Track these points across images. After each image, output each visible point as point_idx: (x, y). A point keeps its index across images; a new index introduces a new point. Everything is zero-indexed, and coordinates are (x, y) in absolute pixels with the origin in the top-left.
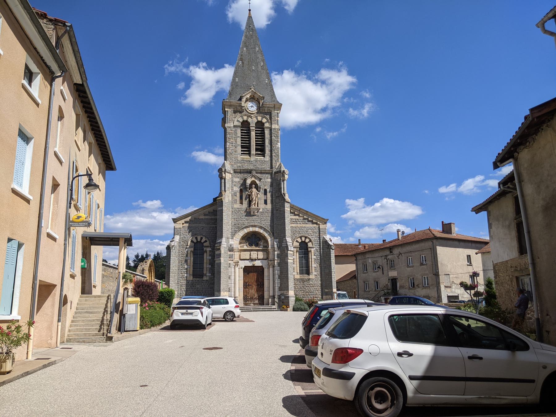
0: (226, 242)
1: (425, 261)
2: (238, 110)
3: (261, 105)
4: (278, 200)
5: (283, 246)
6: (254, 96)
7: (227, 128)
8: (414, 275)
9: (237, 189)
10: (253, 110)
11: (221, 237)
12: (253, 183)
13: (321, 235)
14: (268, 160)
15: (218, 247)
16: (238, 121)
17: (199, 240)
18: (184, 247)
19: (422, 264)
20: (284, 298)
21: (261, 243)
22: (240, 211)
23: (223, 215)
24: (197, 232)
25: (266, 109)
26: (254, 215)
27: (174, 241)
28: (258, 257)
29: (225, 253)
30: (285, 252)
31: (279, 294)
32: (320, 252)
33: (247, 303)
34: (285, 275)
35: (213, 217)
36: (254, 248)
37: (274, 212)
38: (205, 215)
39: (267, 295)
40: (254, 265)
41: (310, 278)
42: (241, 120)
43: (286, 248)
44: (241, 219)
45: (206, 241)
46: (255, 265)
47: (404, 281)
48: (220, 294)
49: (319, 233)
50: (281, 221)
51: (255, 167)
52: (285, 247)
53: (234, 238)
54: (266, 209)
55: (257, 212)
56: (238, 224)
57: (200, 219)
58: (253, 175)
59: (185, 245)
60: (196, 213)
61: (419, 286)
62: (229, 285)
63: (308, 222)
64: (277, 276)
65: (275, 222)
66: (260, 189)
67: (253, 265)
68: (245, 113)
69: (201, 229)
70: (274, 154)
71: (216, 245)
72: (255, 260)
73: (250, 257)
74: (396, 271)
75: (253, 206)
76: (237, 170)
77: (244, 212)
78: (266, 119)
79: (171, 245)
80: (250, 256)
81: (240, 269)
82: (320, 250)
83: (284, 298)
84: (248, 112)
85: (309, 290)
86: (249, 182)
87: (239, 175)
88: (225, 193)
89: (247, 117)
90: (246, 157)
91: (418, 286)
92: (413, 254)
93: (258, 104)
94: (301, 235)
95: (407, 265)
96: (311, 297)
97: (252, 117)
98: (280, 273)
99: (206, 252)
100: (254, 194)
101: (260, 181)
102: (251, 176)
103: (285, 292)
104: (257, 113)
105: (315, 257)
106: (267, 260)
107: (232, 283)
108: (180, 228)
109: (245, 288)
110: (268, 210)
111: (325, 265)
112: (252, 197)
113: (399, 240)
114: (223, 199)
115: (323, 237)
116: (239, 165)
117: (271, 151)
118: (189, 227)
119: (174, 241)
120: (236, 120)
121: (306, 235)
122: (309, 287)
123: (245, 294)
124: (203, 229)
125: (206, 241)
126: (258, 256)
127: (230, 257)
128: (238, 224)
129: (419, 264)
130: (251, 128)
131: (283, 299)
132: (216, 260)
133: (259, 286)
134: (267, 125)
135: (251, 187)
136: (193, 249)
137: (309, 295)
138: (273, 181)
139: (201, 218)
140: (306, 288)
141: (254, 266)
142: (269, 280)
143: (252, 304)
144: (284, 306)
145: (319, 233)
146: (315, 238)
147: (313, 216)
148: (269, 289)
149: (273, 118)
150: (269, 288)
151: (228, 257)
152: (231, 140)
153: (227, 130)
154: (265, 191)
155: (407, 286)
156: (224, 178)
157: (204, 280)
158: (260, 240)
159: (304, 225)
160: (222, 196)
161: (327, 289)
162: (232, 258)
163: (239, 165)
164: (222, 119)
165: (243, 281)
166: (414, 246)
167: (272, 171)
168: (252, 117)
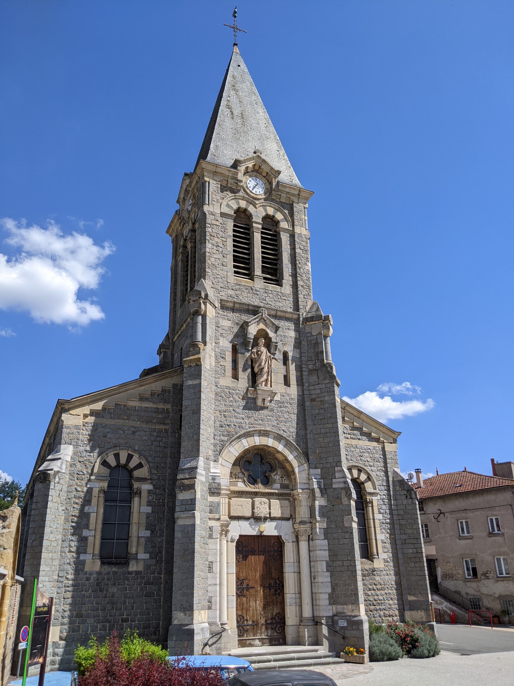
1: (498, 526)
2: (229, 185)
3: (274, 186)
4: (316, 377)
5: (334, 486)
6: (260, 167)
7: (207, 213)
8: (476, 554)
9: (226, 345)
10: (258, 193)
11: (195, 453)
12: (262, 334)
13: (388, 465)
14: (288, 292)
15: (186, 482)
16: (228, 206)
17: (123, 460)
18: (83, 476)
19: (491, 534)
20: (345, 625)
21: (276, 476)
22: (233, 393)
23: (200, 398)
24: (120, 441)
25: (282, 195)
26: (263, 408)
27: (60, 459)
28: (270, 513)
30: (341, 503)
31: (331, 614)
32: (390, 505)
34: (346, 563)
35: (159, 407)
36: (260, 488)
37: (308, 404)
38: (142, 399)
39: (294, 614)
40: (262, 532)
41: (375, 567)
42: (235, 207)
43: (343, 492)
44: (236, 414)
45: (140, 466)
46: (265, 533)
47: (451, 564)
48: (192, 619)
49: (385, 463)
50: (326, 426)
51: (264, 302)
52: (341, 488)
53: (220, 460)
54: (288, 395)
55: (271, 401)
56: (228, 425)
57: (128, 409)
58: (264, 316)
59: (87, 472)
60: (120, 393)
61: (488, 575)
62: (210, 588)
63: (361, 435)
64: (322, 566)
65: (309, 428)
66: (276, 351)
67: (259, 534)
68: (241, 193)
69: (130, 432)
70: (300, 283)
71: (180, 476)
72: (265, 519)
73: (253, 513)
74: (433, 545)
75: (262, 387)
76: (227, 301)
77: (241, 397)
78: (283, 215)
79: (52, 470)
80: (253, 508)
81: (229, 543)
82: (390, 500)
83: (345, 625)
84: (247, 194)
85: (376, 597)
86: (253, 330)
87: (230, 315)
88: (206, 347)
89: (245, 202)
90: (245, 281)
91: (485, 574)
92: (470, 514)
93: (268, 184)
94: (351, 464)
95: (458, 535)
96: (380, 616)
97: (256, 204)
98: (329, 556)
99: (139, 493)
100: (264, 358)
101: (276, 332)
102: (257, 320)
103: (348, 610)
104: (265, 199)
105: (380, 516)
106: (290, 522)
108: (77, 427)
110: (292, 399)
111: (404, 537)
112: (260, 365)
113: (420, 487)
114: (201, 361)
115: (394, 470)
116: (230, 292)
117: (294, 276)
118: (95, 427)
119: (60, 459)
120: (224, 203)
121: (360, 465)
122: (374, 590)
123: (240, 613)
124: (134, 433)
125: (140, 466)
126: (270, 509)
127: (211, 510)
128: (228, 425)
129: (485, 534)
130: (254, 225)
131: (342, 628)
132: (178, 518)
134: (284, 225)
135: (256, 343)
136: (105, 485)
137: (376, 610)
138: (300, 337)
139: (132, 406)
141: (260, 537)
143: (257, 642)
144: (352, 649)
145: (385, 463)
146: (378, 473)
147: (372, 423)
149: (296, 213)
152: (216, 239)
153: (208, 217)
154: (285, 355)
155: (459, 574)
156: (202, 313)
157: (130, 573)
158: (272, 469)
160: (199, 353)
161: (414, 595)
163: (230, 292)
164: (176, 211)
165: (235, 575)
166: (470, 499)
167: (299, 315)
168: (256, 204)
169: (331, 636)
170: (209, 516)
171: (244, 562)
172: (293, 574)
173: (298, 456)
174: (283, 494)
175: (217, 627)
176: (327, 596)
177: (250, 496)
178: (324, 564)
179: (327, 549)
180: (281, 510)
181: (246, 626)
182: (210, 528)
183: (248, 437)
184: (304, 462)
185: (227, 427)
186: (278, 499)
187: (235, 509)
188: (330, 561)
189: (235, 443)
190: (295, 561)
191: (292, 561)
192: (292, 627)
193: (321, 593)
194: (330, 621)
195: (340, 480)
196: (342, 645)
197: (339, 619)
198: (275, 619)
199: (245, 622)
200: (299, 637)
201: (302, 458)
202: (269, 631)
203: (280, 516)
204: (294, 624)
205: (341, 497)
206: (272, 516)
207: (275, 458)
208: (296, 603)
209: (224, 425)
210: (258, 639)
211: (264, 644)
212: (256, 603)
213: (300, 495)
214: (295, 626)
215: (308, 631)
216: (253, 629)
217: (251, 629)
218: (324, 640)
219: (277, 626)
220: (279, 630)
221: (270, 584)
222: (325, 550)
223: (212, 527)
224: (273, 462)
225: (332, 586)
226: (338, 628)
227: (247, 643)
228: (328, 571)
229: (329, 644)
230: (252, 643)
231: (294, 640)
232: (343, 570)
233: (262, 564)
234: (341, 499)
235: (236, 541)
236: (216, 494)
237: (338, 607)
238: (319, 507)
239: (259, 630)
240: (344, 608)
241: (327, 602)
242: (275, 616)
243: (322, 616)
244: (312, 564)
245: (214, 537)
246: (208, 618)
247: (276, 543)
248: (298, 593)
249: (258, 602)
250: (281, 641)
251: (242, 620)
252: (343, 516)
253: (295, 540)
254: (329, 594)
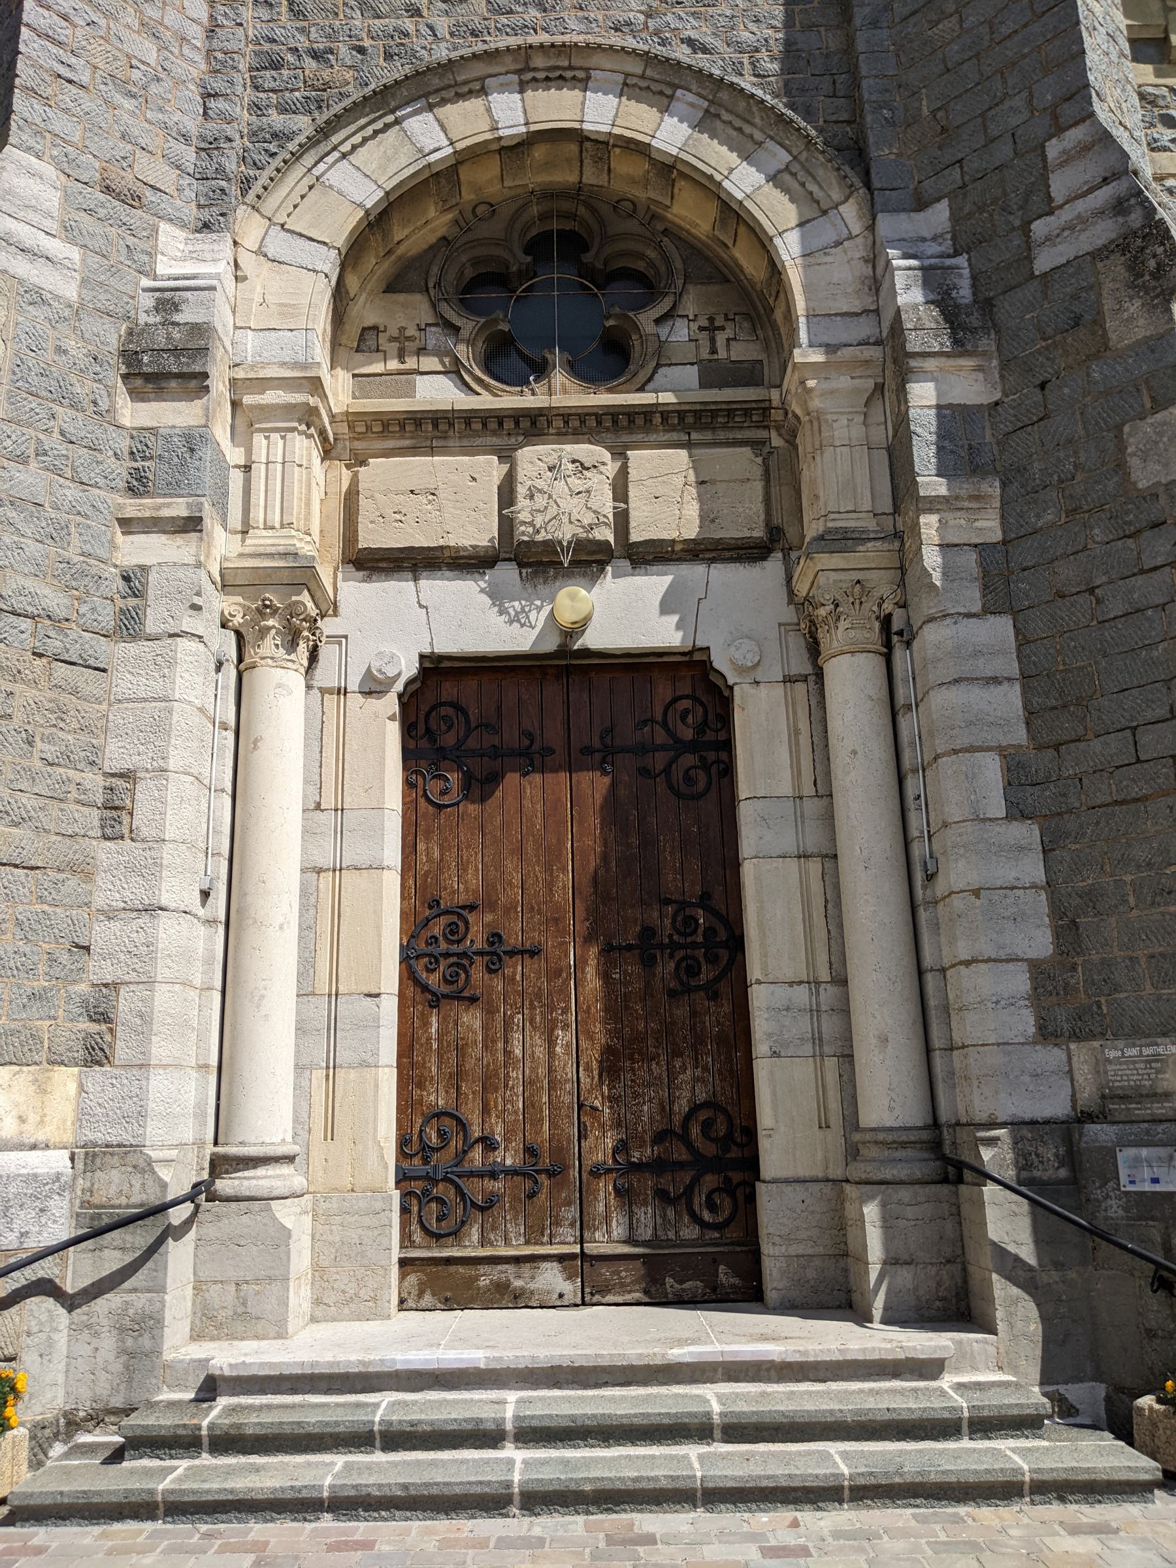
5: (1044, 262)
28: (622, 520)
31: (1056, 1106)
33: (470, 1248)
40: (571, 633)
52: (1099, 254)
62: (102, 934)
67: (550, 645)
73: (507, 525)
81: (355, 700)
98: (1031, 715)
106: (774, 566)
107: (153, 910)
109: (436, 1001)
123: (437, 1098)
128: (315, 55)
133: (666, 968)
142: (832, 856)
143: (551, 1278)
148: (844, 1010)
150: (828, 994)
151: (121, 470)
162: (173, 489)
169: (1059, 1266)
170: (120, 507)
171: (472, 809)
172: (793, 864)
173: (796, 167)
174: (714, 414)
175: (137, 1182)
176: (1019, 982)
177: (495, 440)
178: (991, 770)
179: (1014, 669)
180: (701, 499)
181: (481, 1175)
182: (126, 579)
183: (444, 102)
184: (836, 196)
185: (310, 64)
186: (688, 445)
187: (388, 512)
188: (1040, 748)
189: (357, 139)
190: (808, 789)
191: (786, 789)
192: (788, 1189)
193: (967, 963)
194: (1049, 1153)
195: (1081, 206)
196: (1151, 1334)
197: (1124, 1143)
198: (685, 1139)
199: (477, 1154)
200: (846, 1255)
201: (820, 173)
202: (646, 1216)
203: (691, 531)
204: (803, 1172)
205: (1100, 312)
206: (635, 537)
207: (665, 232)
208: (818, 1039)
209: (290, 58)
210: (561, 1258)
211: (604, 1290)
212: (551, 1042)
213: (811, 383)
214: (815, 1187)
215: (888, 1224)
216: (531, 1195)
217: (514, 1198)
218: (1002, 1290)
219: (696, 1180)
220: (712, 1207)
221: (648, 932)
222: (995, 680)
223: (144, 569)
224: (652, 254)
225: (1057, 911)
226: (1115, 1209)
227: (484, 1282)
228: (1016, 812)
229: (1045, 1319)
230: (518, 1283)
231: (811, 1274)
232: (1135, 791)
233: (594, 822)
234: (1098, 321)
235: (399, 686)
236: (173, 384)
237: (1113, 1054)
238: (939, 416)
239: (569, 1204)
240: (1156, 1058)
241: (1025, 1022)
242: (688, 1118)
243: (981, 1116)
244: (913, 786)
245: (151, 627)
246: (82, 1116)
247: (685, 704)
248: (833, 981)
249: (563, 1038)
250: (724, 1275)
251: (456, 1143)
252: (1119, 428)
253: (800, 664)
254: (1036, 968)
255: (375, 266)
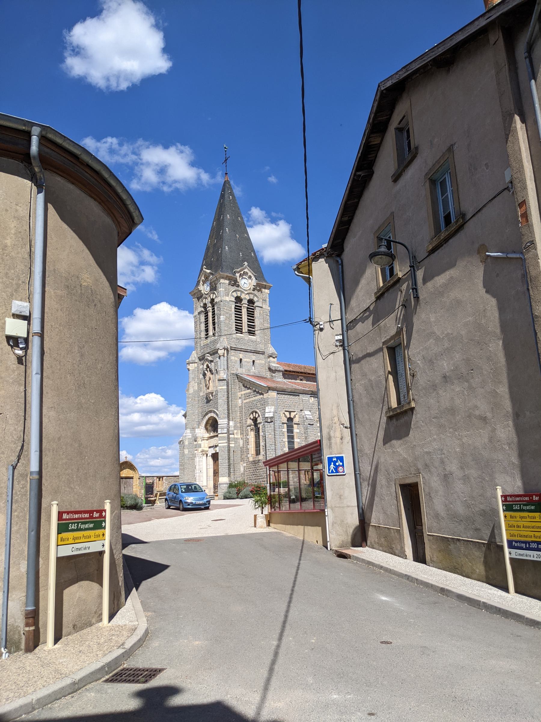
0: (191, 433)
26: (211, 400)
29: (190, 443)
53: (200, 427)
140: (257, 471)
159: (254, 398)
255: (209, 425)
